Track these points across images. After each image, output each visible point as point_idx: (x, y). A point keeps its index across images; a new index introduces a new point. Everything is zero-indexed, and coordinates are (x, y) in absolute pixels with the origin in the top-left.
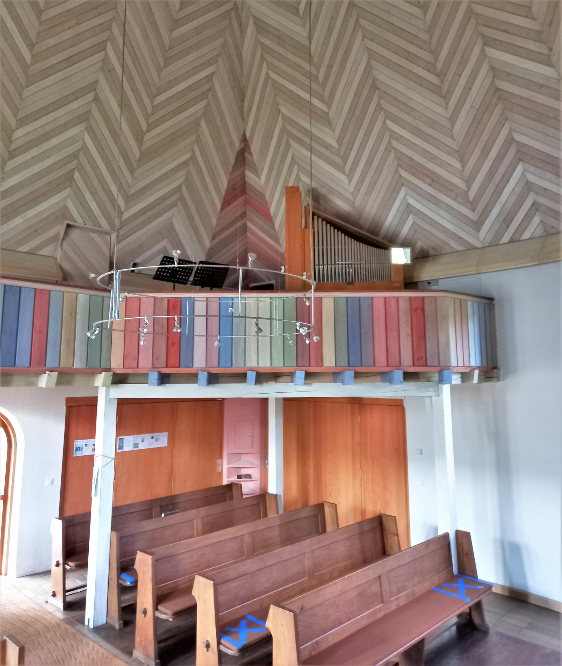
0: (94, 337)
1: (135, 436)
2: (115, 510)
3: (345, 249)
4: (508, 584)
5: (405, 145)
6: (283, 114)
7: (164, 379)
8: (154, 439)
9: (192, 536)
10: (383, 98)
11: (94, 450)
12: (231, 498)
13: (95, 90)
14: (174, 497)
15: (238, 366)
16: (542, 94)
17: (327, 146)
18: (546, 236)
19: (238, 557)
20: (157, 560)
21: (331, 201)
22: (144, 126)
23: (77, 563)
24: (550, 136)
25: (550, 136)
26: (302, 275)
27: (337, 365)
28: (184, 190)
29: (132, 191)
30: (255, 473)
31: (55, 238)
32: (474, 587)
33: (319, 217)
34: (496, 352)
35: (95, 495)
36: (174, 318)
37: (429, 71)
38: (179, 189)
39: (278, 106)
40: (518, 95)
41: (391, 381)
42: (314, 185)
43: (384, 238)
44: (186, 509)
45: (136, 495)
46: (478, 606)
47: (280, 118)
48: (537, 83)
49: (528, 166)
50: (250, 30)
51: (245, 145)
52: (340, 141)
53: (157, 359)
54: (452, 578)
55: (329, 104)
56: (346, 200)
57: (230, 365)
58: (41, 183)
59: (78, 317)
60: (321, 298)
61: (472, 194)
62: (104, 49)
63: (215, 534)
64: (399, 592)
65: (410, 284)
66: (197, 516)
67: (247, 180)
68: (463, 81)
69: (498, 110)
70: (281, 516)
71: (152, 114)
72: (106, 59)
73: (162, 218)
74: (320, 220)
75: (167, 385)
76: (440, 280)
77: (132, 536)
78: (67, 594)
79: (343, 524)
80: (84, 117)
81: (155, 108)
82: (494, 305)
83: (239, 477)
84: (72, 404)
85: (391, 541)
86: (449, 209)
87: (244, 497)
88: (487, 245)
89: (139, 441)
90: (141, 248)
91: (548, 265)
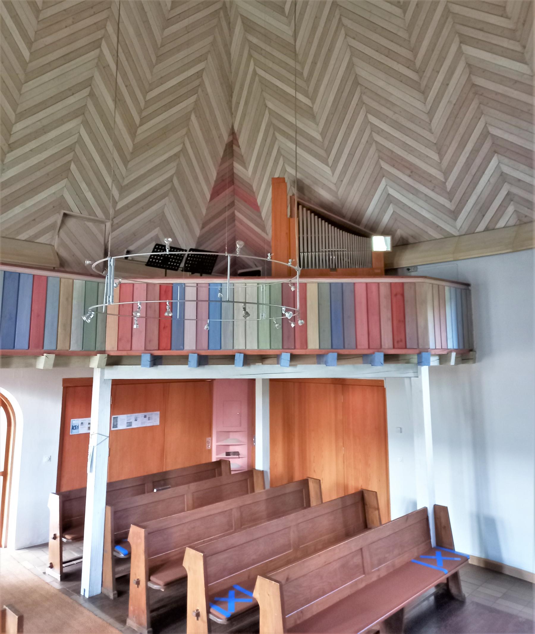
0: (89, 321)
1: (129, 415)
2: (110, 485)
3: (329, 237)
4: (483, 556)
5: (386, 138)
6: (269, 108)
7: (156, 361)
8: (147, 418)
9: (183, 510)
10: (364, 93)
11: (89, 428)
12: (220, 474)
13: (90, 86)
14: (166, 473)
15: (226, 348)
16: (516, 90)
17: (311, 139)
18: (520, 225)
19: (227, 531)
20: (149, 533)
21: (315, 191)
22: (137, 120)
23: (73, 536)
24: (524, 130)
25: (524, 130)
26: (288, 262)
27: (321, 347)
28: (175, 181)
29: (126, 182)
30: (243, 450)
31: (52, 227)
32: (451, 558)
33: (303, 206)
34: (472, 335)
35: (91, 471)
36: (166, 302)
37: (408, 68)
38: (170, 180)
39: (264, 100)
40: (493, 91)
41: (372, 363)
42: (299, 176)
43: (366, 226)
44: (177, 485)
45: (129, 472)
46: (455, 577)
47: (267, 112)
48: (511, 79)
49: (503, 158)
50: (238, 28)
51: (233, 138)
52: (323, 134)
53: (150, 341)
54: (430, 551)
55: (313, 99)
56: (329, 190)
57: (219, 348)
58: (39, 174)
59: (75, 302)
60: (306, 284)
61: (449, 185)
62: (99, 46)
63: (205, 508)
64: (380, 563)
65: (390, 270)
66: (188, 491)
67: (235, 171)
68: (440, 77)
69: (474, 105)
70: (267, 491)
71: (145, 108)
72: (101, 57)
73: (154, 208)
74: (305, 209)
75: (159, 366)
76: (418, 267)
77: (126, 510)
78: (64, 565)
79: (326, 498)
80: (80, 112)
81: (148, 103)
82: (470, 290)
83: (228, 454)
84: (69, 385)
85: (372, 515)
86: (428, 199)
87: (232, 473)
88: (463, 233)
89: (132, 420)
90: (135, 236)
91: (522, 253)
